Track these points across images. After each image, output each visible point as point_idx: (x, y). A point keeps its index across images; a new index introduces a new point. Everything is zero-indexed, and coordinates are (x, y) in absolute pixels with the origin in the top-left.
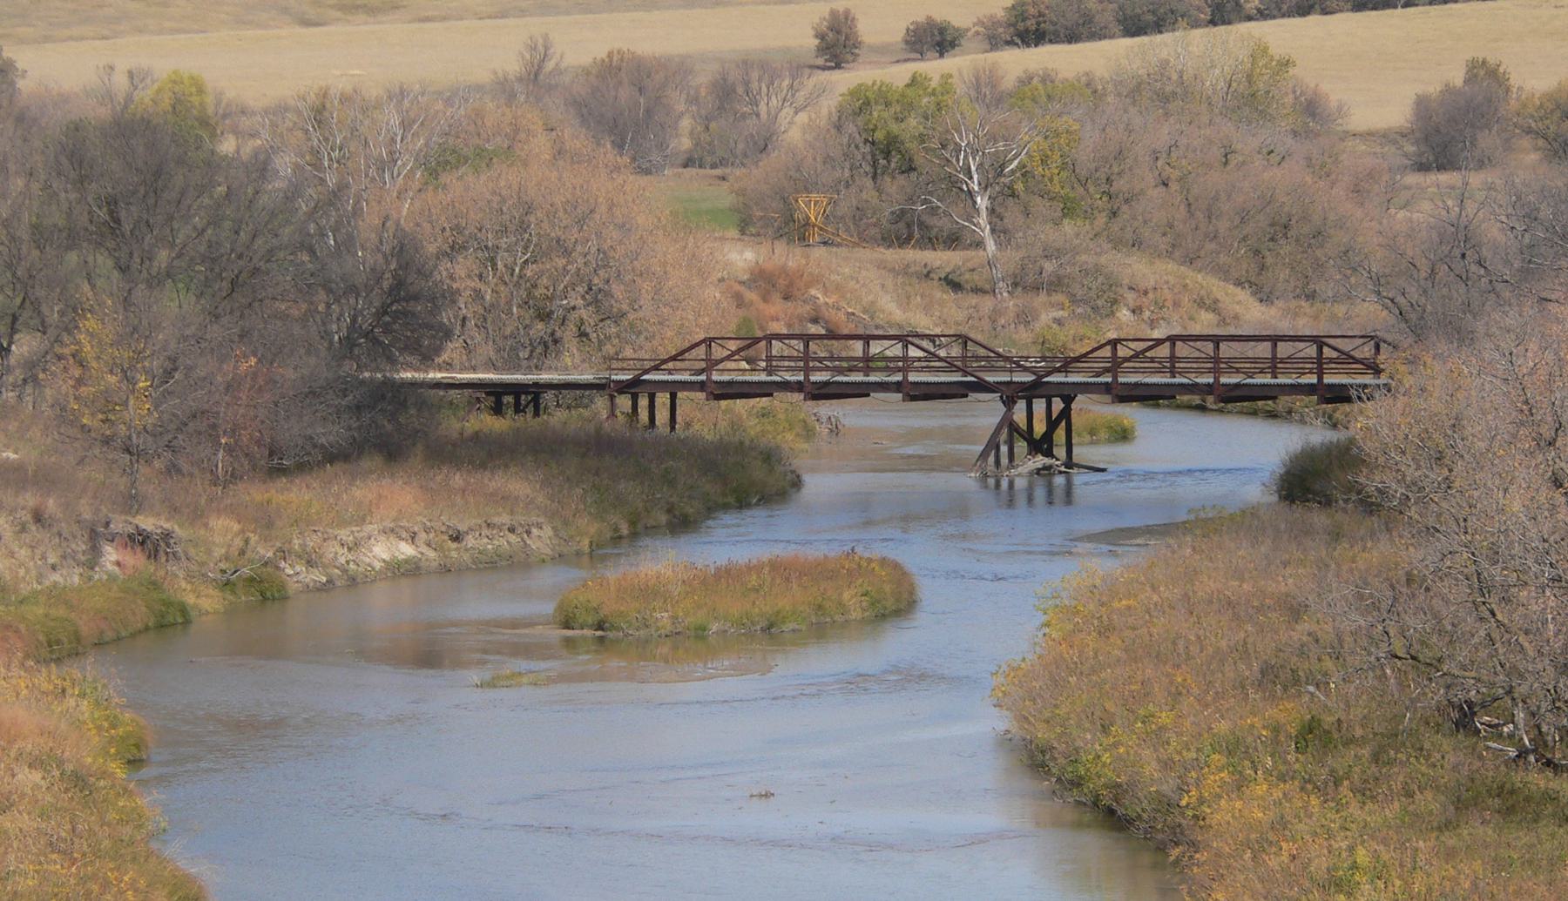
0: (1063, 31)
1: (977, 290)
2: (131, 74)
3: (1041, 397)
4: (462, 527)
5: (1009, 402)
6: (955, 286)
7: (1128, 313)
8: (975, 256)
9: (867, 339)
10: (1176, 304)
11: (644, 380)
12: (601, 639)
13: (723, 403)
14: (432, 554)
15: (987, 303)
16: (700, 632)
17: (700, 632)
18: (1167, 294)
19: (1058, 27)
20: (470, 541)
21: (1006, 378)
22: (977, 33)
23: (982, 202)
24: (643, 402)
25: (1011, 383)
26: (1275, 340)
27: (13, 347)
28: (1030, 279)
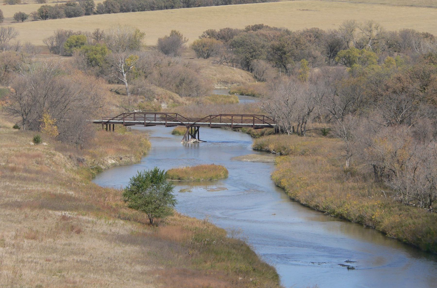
0: (52, 16)
1: (123, 94)
3: (193, 126)
5: (188, 128)
6: (118, 93)
7: (156, 100)
8: (121, 86)
9: (155, 114)
11: (110, 122)
12: (179, 182)
14: (117, 162)
16: (199, 180)
17: (199, 180)
18: (163, 96)
19: (51, 15)
20: (123, 159)
21: (188, 123)
22: (31, 16)
23: (125, 75)
24: (108, 125)
25: (188, 124)
26: (242, 116)
28: (135, 92)
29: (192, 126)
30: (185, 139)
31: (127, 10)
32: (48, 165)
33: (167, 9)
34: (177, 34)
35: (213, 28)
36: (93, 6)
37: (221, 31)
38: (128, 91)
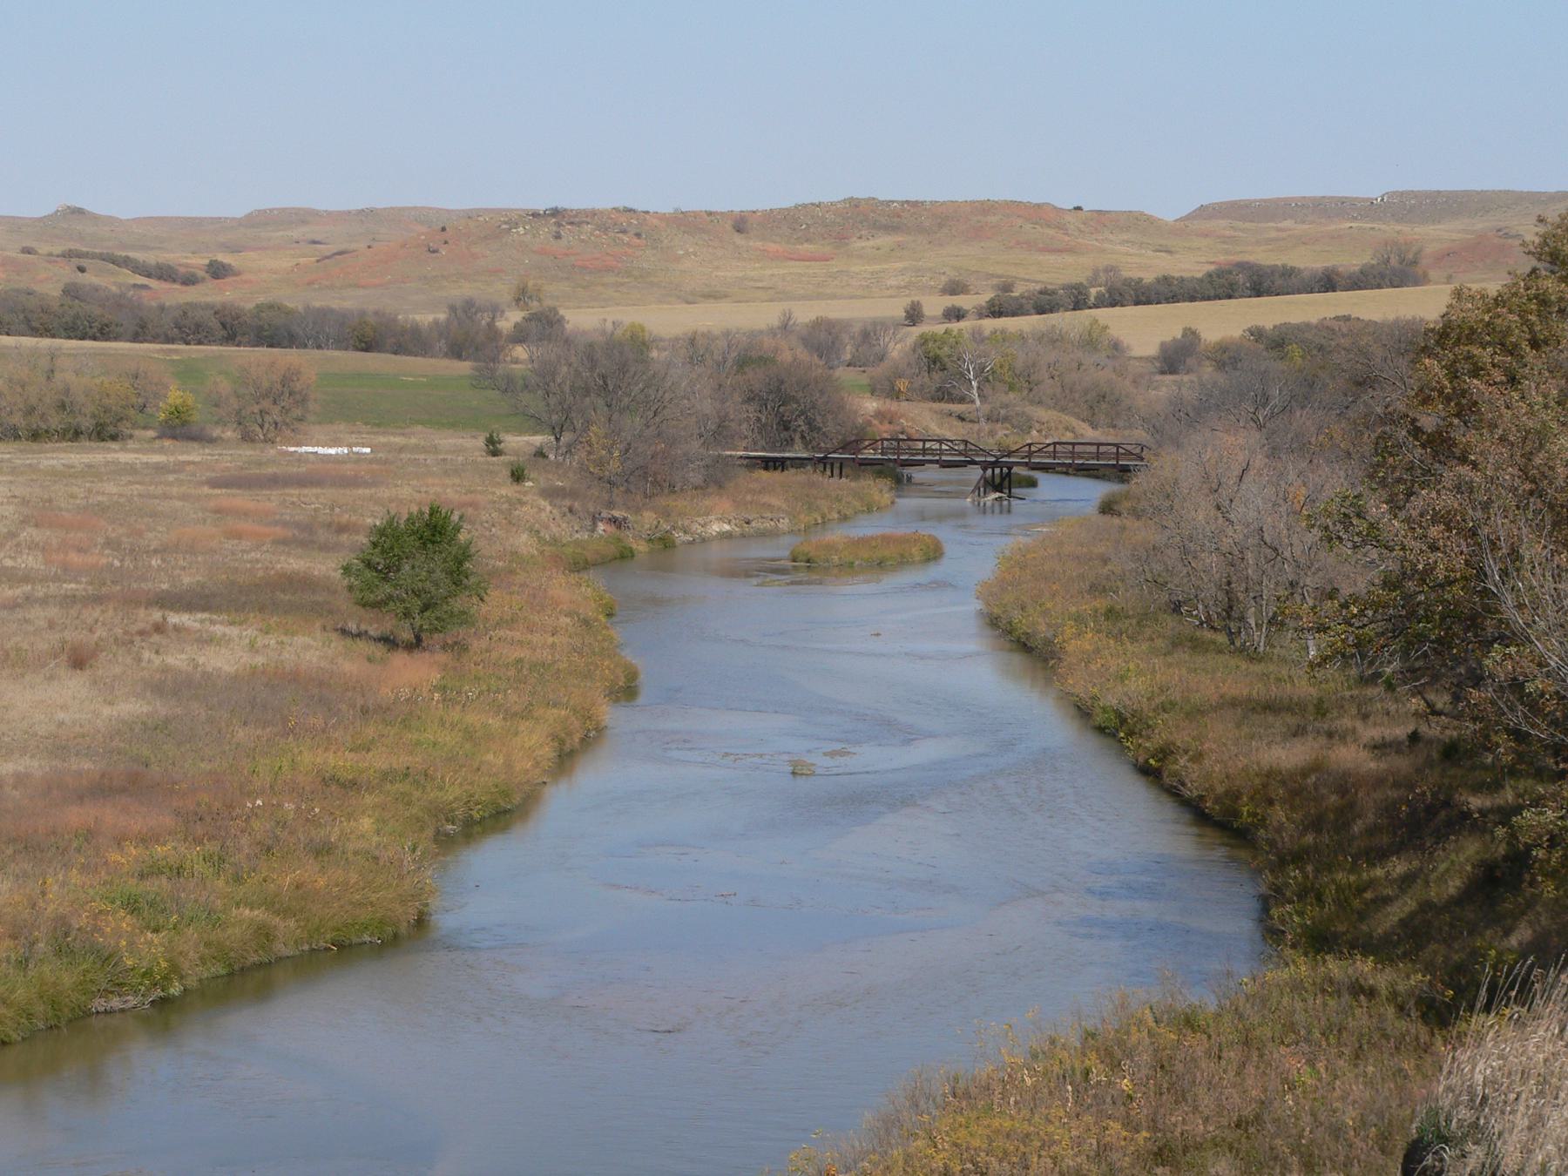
1: (971, 421)
2: (614, 323)
4: (751, 518)
5: (985, 469)
6: (963, 419)
14: (737, 529)
15: (976, 427)
20: (754, 524)
29: (994, 465)
30: (977, 493)
31: (1148, 302)
32: (486, 525)
33: (1220, 299)
34: (1194, 333)
35: (1260, 324)
36: (1087, 296)
37: (1275, 327)
38: (980, 414)
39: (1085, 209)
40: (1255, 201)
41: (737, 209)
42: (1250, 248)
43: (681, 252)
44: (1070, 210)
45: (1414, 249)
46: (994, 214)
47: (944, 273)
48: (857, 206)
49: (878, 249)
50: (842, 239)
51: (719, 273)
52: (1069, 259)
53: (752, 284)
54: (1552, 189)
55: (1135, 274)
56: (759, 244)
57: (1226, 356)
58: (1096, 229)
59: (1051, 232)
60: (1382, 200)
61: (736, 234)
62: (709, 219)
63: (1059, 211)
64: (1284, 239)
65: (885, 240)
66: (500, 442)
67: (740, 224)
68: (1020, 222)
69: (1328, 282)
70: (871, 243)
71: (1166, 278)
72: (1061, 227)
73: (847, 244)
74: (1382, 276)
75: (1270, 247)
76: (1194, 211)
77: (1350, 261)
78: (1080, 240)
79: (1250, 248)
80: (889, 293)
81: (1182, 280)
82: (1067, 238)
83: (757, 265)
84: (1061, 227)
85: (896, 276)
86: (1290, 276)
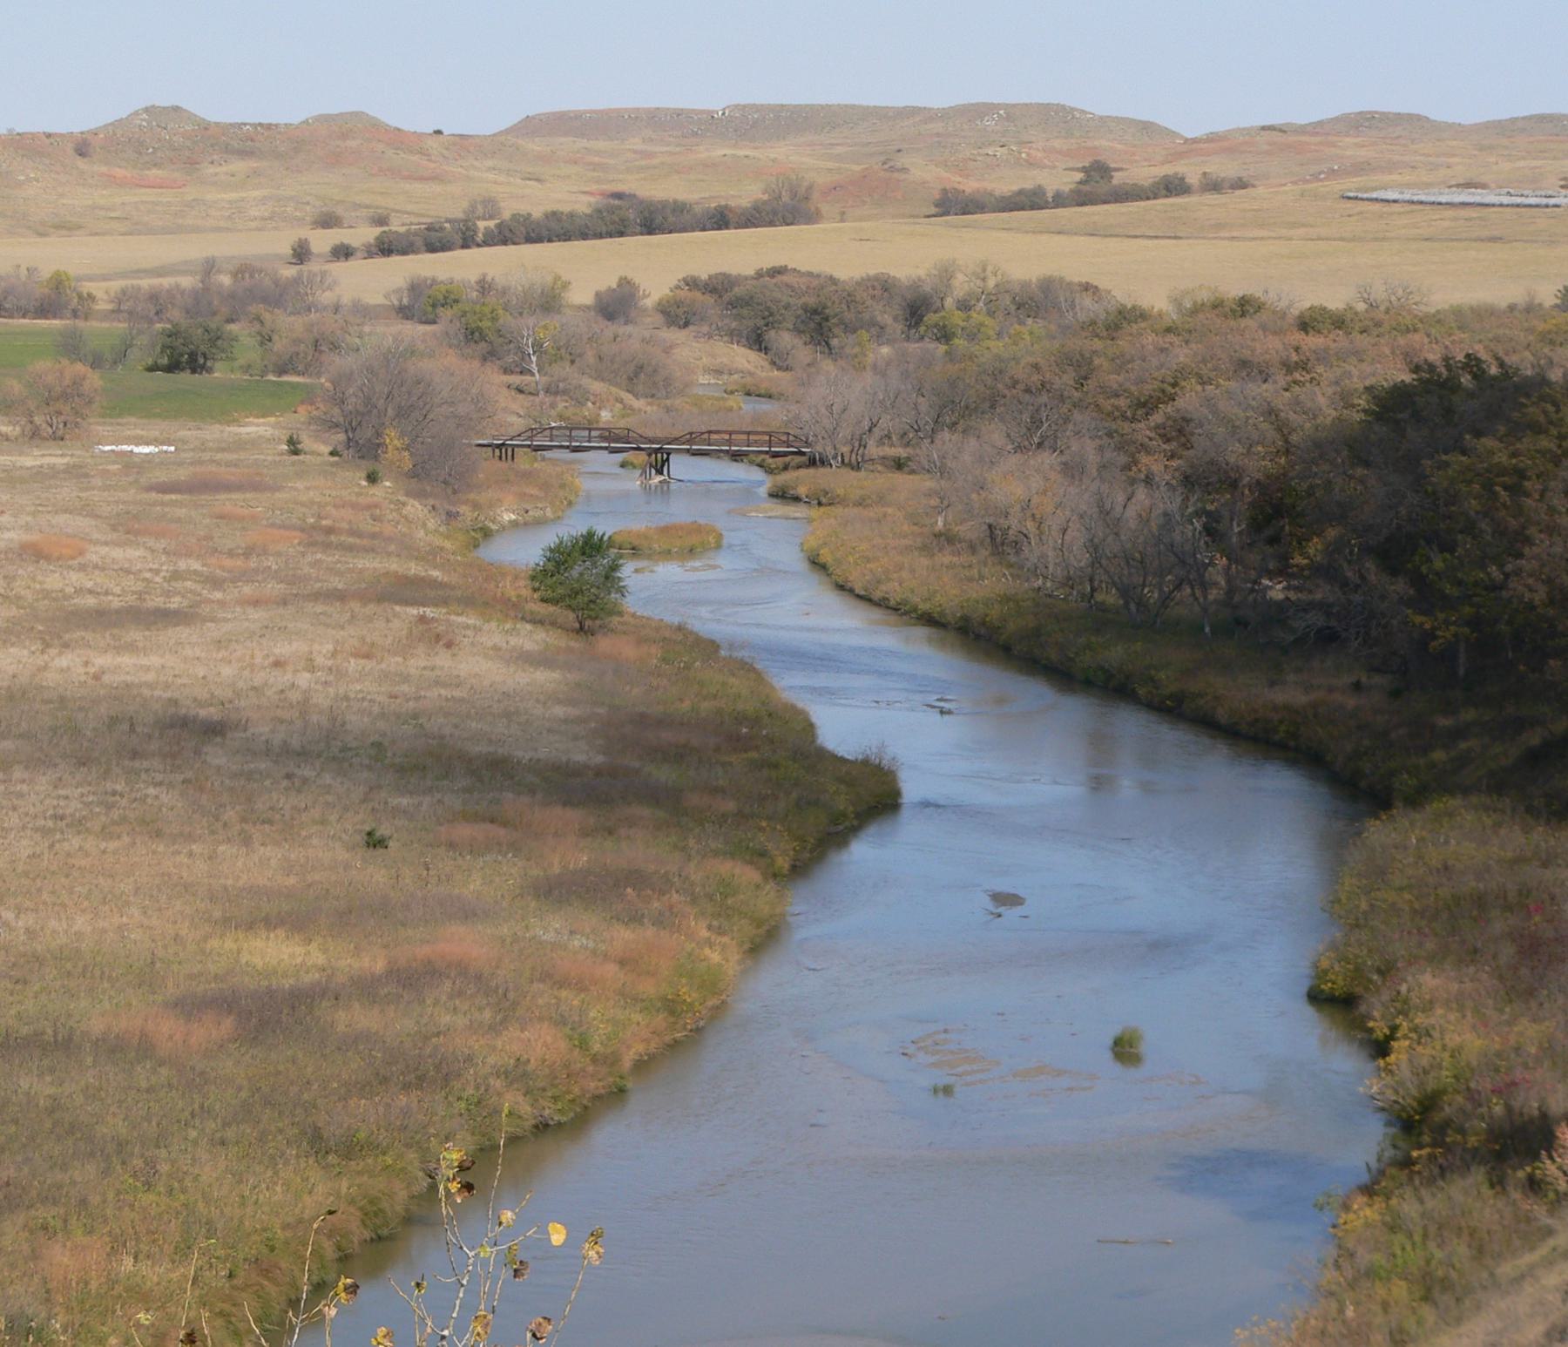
1: (531, 394)
2: (28, 269)
5: (650, 455)
6: (521, 391)
9: (590, 430)
10: (608, 401)
13: (539, 452)
15: (537, 400)
20: (530, 513)
23: (534, 358)
24: (503, 450)
27: (967, 538)
31: (539, 240)
33: (611, 237)
39: (445, 133)
40: (586, 112)
41: (76, 129)
42: (621, 177)
43: (22, 178)
44: (430, 134)
45: (805, 184)
46: (354, 138)
47: (308, 203)
48: (206, 129)
49: (233, 176)
50: (192, 163)
51: (65, 201)
52: (437, 188)
53: (102, 213)
54: (900, 103)
55: (523, 208)
56: (104, 169)
57: (680, 311)
58: (460, 155)
59: (415, 158)
60: (723, 114)
61: (79, 157)
62: (47, 141)
63: (420, 136)
64: (655, 167)
65: (239, 166)
66: (299, 443)
67: (82, 147)
68: (381, 147)
69: (721, 220)
70: (224, 169)
71: (554, 213)
72: (423, 152)
73: (198, 170)
74: (775, 213)
75: (643, 175)
76: (520, 122)
77: (745, 194)
78: (445, 167)
79: (621, 177)
80: (253, 224)
81: (571, 215)
82: (433, 165)
83: (104, 192)
84: (423, 152)
85: (257, 206)
86: (682, 211)
